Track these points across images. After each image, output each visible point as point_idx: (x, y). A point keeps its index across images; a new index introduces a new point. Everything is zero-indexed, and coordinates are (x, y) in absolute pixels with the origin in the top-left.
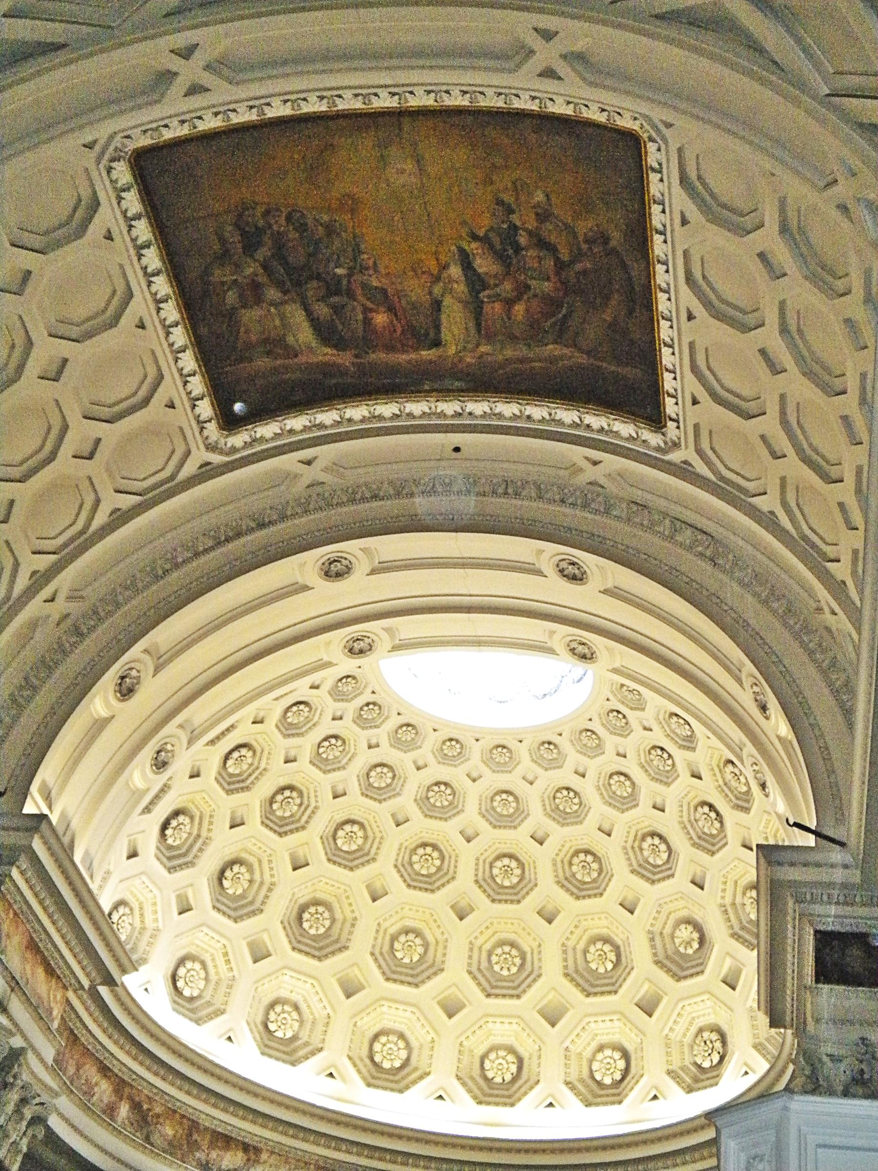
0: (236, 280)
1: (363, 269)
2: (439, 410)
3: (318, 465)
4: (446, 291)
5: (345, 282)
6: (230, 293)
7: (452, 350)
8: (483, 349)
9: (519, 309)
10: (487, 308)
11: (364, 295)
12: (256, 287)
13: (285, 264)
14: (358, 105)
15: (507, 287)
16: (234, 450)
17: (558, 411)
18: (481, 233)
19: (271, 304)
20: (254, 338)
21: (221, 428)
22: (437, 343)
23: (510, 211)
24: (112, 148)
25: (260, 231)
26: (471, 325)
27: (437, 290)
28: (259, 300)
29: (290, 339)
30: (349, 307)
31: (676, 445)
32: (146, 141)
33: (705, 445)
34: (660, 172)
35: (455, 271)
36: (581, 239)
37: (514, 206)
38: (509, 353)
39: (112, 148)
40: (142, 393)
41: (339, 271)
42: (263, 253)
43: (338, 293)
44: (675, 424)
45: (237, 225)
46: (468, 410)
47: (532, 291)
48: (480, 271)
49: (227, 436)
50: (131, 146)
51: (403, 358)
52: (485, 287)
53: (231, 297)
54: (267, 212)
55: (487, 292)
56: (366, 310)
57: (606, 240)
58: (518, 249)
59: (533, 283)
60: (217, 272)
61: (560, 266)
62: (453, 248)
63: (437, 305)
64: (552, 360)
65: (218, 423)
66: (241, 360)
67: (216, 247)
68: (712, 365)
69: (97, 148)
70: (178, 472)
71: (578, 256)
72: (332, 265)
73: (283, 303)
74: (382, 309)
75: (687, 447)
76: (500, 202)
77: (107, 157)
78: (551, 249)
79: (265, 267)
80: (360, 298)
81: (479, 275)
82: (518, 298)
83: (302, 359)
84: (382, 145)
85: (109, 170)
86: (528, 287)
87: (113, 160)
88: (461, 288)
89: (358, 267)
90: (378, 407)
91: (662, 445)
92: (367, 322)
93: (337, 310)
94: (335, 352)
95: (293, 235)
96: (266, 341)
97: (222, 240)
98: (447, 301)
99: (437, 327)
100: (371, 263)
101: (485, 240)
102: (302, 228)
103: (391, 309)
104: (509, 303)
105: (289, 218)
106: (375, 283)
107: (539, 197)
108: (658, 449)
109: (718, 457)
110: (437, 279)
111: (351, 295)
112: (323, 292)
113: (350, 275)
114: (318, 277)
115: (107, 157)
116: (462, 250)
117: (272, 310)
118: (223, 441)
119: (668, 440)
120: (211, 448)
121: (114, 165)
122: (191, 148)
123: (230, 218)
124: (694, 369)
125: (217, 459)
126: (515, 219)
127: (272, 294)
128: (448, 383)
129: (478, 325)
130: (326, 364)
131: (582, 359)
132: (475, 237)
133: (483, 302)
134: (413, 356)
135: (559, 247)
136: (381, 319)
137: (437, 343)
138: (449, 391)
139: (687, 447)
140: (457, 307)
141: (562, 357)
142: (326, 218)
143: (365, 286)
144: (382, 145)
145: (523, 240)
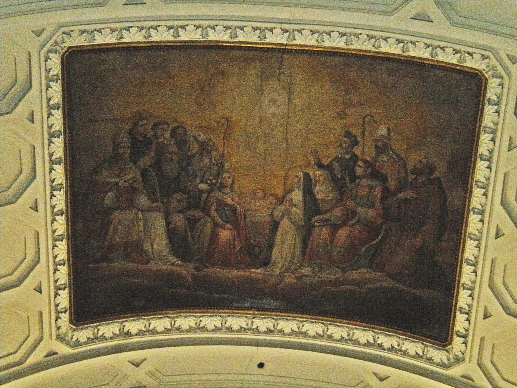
0: (117, 183)
1: (222, 186)
2: (254, 326)
3: (145, 367)
4: (287, 213)
5: (205, 195)
6: (109, 194)
7: (277, 271)
8: (306, 270)
9: (343, 233)
10: (316, 231)
11: (217, 210)
12: (132, 190)
13: (161, 175)
14: (254, 38)
15: (337, 212)
16: (78, 344)
17: (355, 331)
18: (325, 162)
19: (139, 210)
20: (117, 239)
21: (71, 322)
22: (266, 263)
23: (355, 143)
24: (52, 41)
25: (148, 142)
26: (299, 245)
27: (278, 213)
28: (131, 204)
29: (147, 247)
30: (203, 220)
31: (459, 360)
32: (80, 41)
33: (486, 361)
34: (497, 104)
35: (297, 196)
36: (409, 168)
37: (359, 139)
38: (325, 276)
39: (52, 41)
40: (17, 274)
41: (203, 186)
42: (146, 161)
43: (197, 207)
44: (462, 340)
45: (130, 132)
46: (279, 328)
47: (357, 218)
48: (318, 196)
49: (74, 331)
50: (70, 42)
51: (235, 274)
52: (318, 212)
53: (109, 197)
54: (156, 125)
55: (317, 218)
56: (216, 225)
57: (431, 169)
58: (354, 178)
59: (359, 209)
60: (105, 173)
61: (387, 193)
62: (301, 174)
63: (275, 225)
64: (360, 283)
65: (70, 316)
66: (105, 259)
67: (110, 150)
68: (507, 282)
69: (44, 36)
70: (27, 358)
71: (401, 188)
72: (198, 181)
73: (150, 210)
74: (228, 226)
75: (470, 361)
76: (348, 134)
77: (48, 46)
78: (383, 179)
79: (144, 173)
80: (213, 213)
81: (316, 200)
82: (344, 224)
83: (152, 266)
84: (263, 77)
85: (47, 59)
86: (354, 213)
87: (50, 51)
88: (298, 212)
89: (218, 185)
90: (204, 319)
91: (446, 361)
92: (214, 235)
93: (192, 222)
94: (179, 262)
95: (174, 148)
96: (127, 244)
97: (116, 146)
98: (285, 224)
99: (271, 246)
100: (230, 181)
101: (329, 168)
102: (182, 143)
103: (237, 227)
104: (335, 227)
105: (173, 133)
106: (229, 201)
107: (382, 131)
108: (441, 365)
109: (497, 369)
110: (281, 201)
111: (206, 210)
112: (185, 204)
113: (209, 192)
114: (185, 191)
115: (48, 46)
116: (306, 175)
117: (140, 216)
118: (70, 334)
119: (451, 356)
120: (61, 338)
121: (51, 55)
122: (112, 55)
123: (128, 126)
124: (492, 287)
125: (64, 350)
126: (357, 151)
127: (143, 200)
128: (266, 302)
129: (304, 247)
130: (171, 273)
131: (388, 283)
132: (320, 166)
133: (314, 226)
134: (241, 273)
135: (390, 179)
136: (225, 235)
137: (266, 263)
138: (264, 309)
139: (470, 361)
140: (292, 229)
141: (371, 281)
142: (202, 137)
143: (221, 204)
144: (263, 77)
145: (359, 171)
